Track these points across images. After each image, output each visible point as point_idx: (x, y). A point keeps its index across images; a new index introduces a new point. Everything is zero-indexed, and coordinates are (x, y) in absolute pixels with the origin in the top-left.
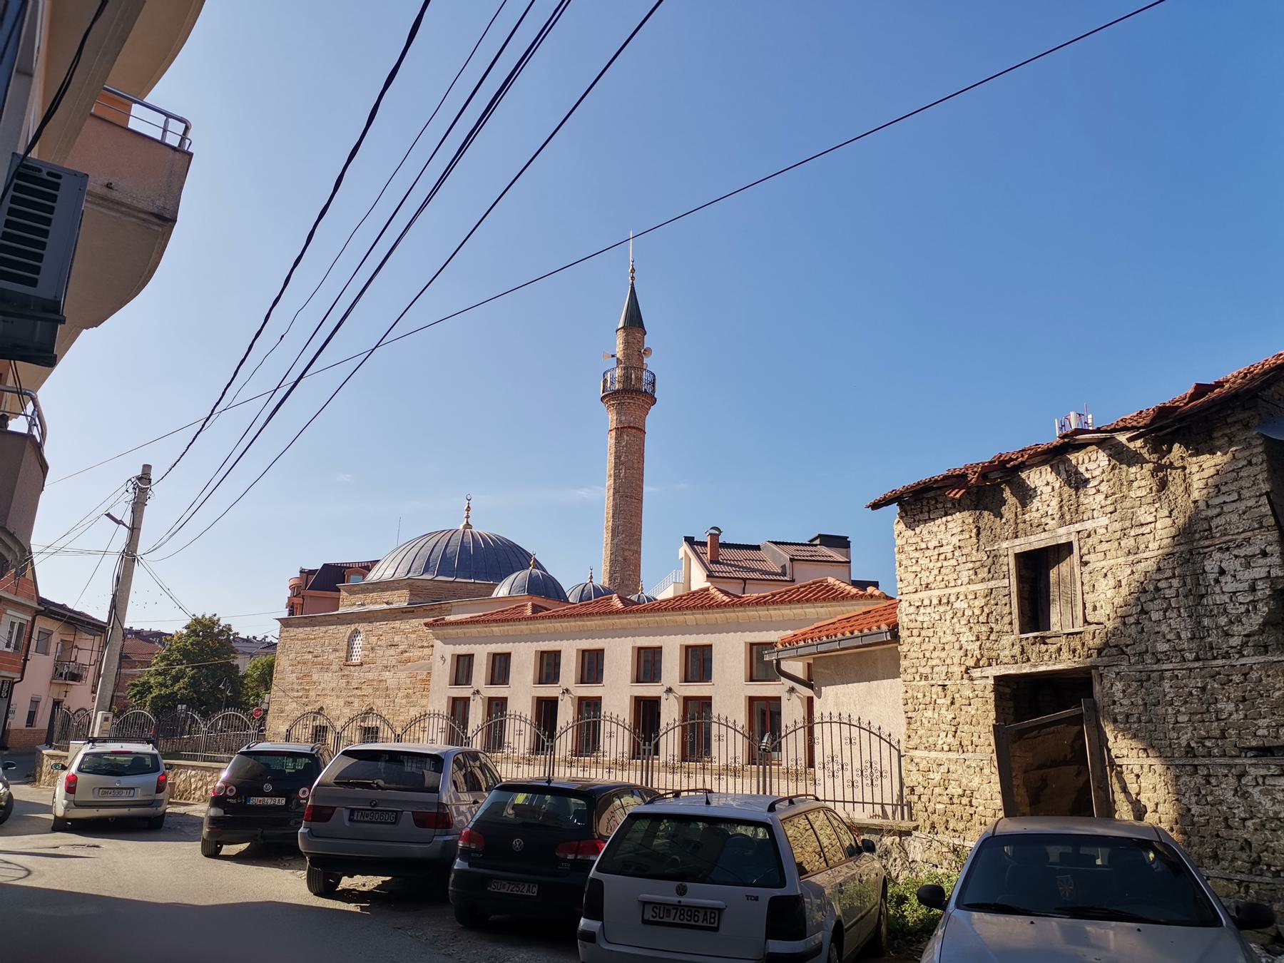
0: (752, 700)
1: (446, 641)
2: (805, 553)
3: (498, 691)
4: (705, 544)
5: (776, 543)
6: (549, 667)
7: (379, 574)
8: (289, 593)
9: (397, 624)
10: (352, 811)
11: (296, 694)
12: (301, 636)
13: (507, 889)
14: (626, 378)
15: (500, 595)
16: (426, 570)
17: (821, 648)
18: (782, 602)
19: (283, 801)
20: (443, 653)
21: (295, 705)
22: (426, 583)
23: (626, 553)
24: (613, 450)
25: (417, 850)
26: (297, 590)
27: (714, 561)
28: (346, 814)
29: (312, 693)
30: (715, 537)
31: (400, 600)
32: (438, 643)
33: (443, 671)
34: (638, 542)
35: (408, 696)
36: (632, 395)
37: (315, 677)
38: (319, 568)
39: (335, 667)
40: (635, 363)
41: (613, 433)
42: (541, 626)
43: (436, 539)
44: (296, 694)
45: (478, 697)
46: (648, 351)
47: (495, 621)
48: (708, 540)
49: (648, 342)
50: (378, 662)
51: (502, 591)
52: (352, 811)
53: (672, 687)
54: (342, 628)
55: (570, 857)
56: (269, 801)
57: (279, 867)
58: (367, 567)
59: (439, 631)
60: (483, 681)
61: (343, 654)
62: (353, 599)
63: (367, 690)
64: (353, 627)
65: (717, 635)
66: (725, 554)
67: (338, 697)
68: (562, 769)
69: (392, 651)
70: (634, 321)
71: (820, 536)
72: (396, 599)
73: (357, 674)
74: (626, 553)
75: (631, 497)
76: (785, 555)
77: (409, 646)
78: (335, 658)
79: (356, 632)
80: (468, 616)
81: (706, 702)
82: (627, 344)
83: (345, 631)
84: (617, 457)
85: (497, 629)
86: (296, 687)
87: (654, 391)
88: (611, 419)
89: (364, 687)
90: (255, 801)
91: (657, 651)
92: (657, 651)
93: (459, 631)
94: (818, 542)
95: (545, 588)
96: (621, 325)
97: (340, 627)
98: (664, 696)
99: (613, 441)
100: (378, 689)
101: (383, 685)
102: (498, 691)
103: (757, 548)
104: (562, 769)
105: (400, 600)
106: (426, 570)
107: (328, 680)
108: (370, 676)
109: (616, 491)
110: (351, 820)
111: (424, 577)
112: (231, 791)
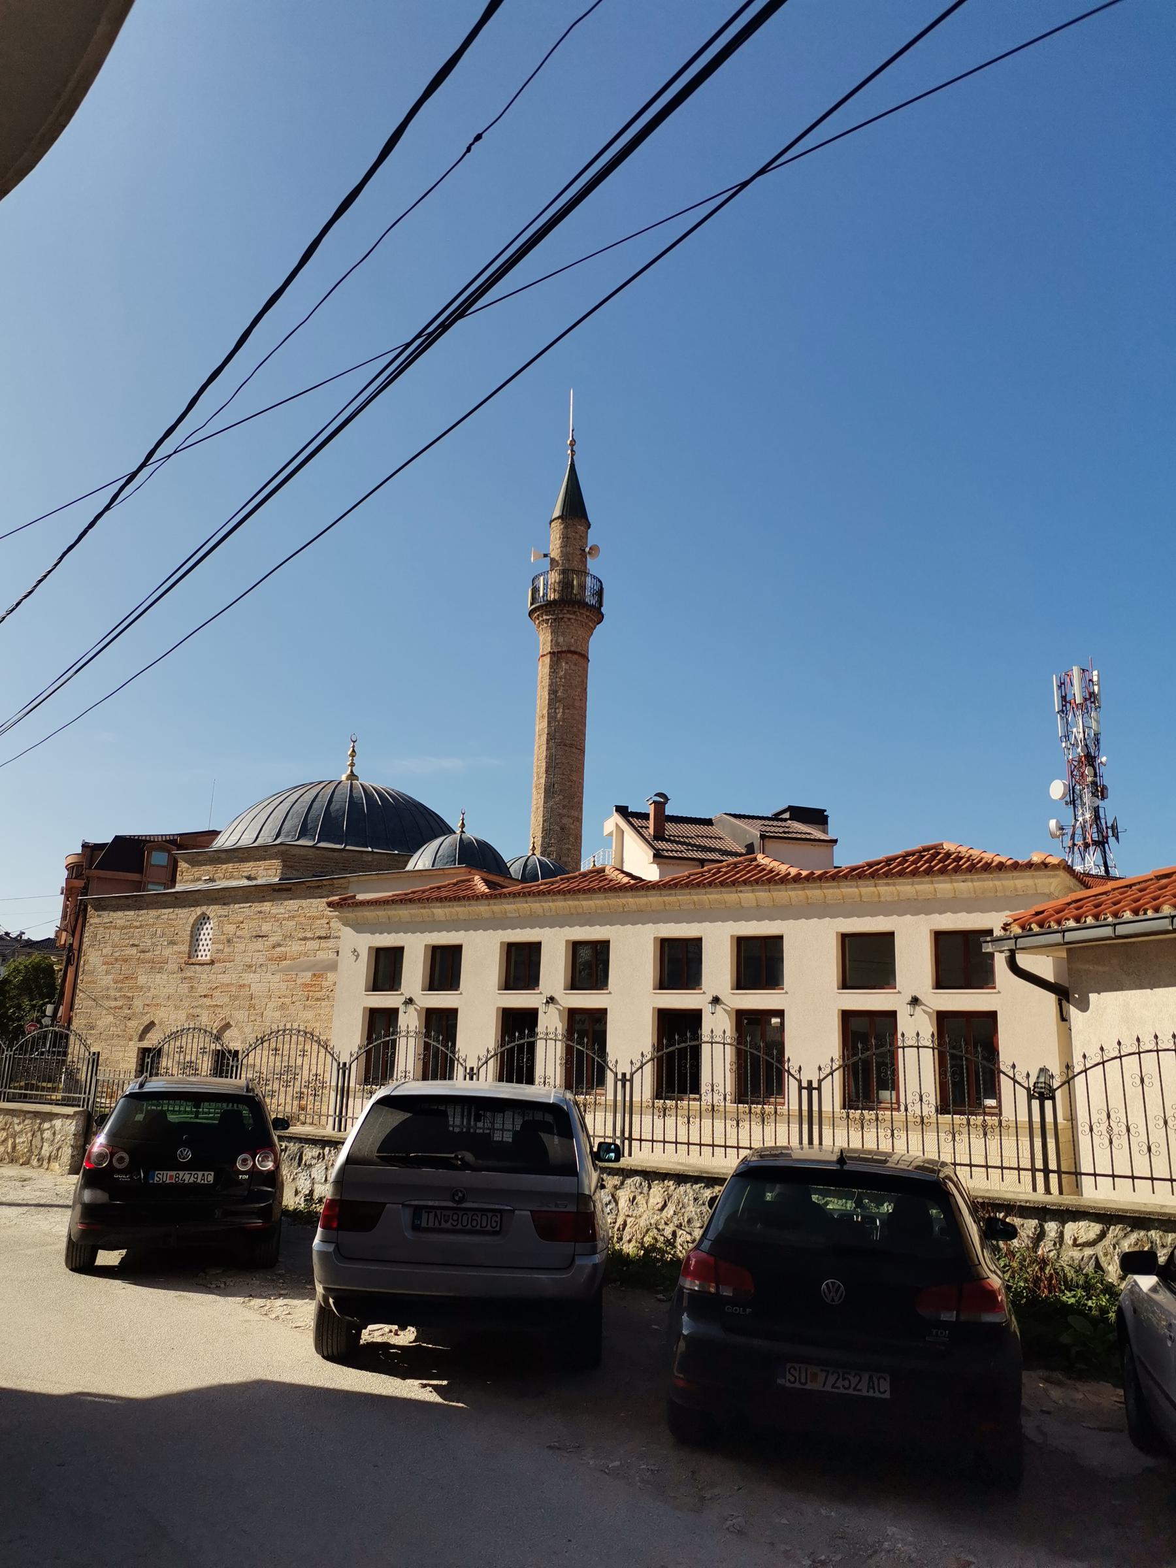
0: (847, 1017)
1: (359, 927)
2: (776, 828)
3: (441, 1000)
4: (645, 816)
5: (735, 816)
6: (521, 965)
7: (234, 839)
8: (65, 873)
9: (266, 906)
10: (417, 1211)
11: (113, 1004)
12: (120, 923)
13: (823, 1382)
14: (565, 585)
15: (420, 867)
16: (304, 832)
17: (1121, 930)
18: (901, 874)
19: (210, 1177)
20: (355, 947)
21: (111, 1018)
22: (304, 852)
23: (565, 821)
24: (546, 682)
25: (545, 1281)
26: (76, 871)
27: (659, 836)
28: (406, 1216)
29: (138, 1003)
30: (660, 806)
31: (268, 873)
32: (347, 933)
33: (354, 972)
34: (579, 806)
35: (283, 1007)
36: (572, 607)
37: (142, 980)
38: (109, 840)
39: (172, 966)
40: (576, 564)
41: (547, 660)
42: (510, 907)
43: (314, 792)
44: (113, 1004)
45: (411, 1008)
46: (595, 550)
47: (440, 900)
48: (651, 810)
49: (593, 537)
50: (238, 959)
51: (421, 860)
52: (417, 1211)
53: (717, 997)
54: (182, 913)
55: (949, 1316)
56: (187, 1177)
57: (209, 1291)
58: (215, 834)
59: (350, 914)
60: (420, 986)
61: (185, 948)
62: (198, 871)
63: (221, 999)
64: (199, 911)
65: (791, 922)
66: (671, 829)
67: (177, 1007)
68: (647, 1119)
69: (259, 944)
70: (574, 509)
71: (790, 809)
72: (261, 872)
73: (205, 977)
74: (565, 821)
75: (571, 746)
76: (753, 831)
77: (285, 937)
78: (174, 954)
79: (204, 918)
80: (390, 894)
81: (598, 1017)
82: (566, 539)
83: (186, 916)
84: (553, 692)
85: (440, 912)
86: (112, 993)
87: (601, 605)
88: (543, 639)
89: (216, 994)
90: (165, 1177)
91: (695, 945)
92: (695, 945)
93: (381, 913)
94: (787, 815)
95: (479, 856)
96: (557, 513)
97: (178, 911)
98: (402, 1009)
99: (547, 670)
100: (236, 998)
101: (245, 992)
102: (441, 1000)
103: (708, 822)
104: (647, 1119)
105: (268, 873)
106: (304, 832)
107: (163, 984)
108: (225, 979)
109: (551, 737)
110: (416, 1228)
111: (299, 843)
112: (121, 1159)
